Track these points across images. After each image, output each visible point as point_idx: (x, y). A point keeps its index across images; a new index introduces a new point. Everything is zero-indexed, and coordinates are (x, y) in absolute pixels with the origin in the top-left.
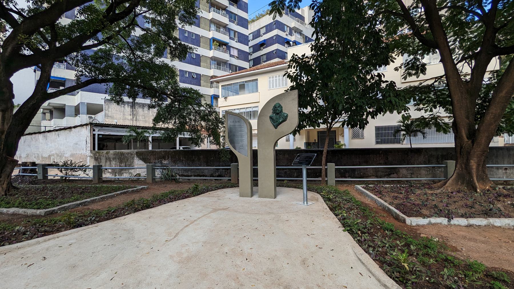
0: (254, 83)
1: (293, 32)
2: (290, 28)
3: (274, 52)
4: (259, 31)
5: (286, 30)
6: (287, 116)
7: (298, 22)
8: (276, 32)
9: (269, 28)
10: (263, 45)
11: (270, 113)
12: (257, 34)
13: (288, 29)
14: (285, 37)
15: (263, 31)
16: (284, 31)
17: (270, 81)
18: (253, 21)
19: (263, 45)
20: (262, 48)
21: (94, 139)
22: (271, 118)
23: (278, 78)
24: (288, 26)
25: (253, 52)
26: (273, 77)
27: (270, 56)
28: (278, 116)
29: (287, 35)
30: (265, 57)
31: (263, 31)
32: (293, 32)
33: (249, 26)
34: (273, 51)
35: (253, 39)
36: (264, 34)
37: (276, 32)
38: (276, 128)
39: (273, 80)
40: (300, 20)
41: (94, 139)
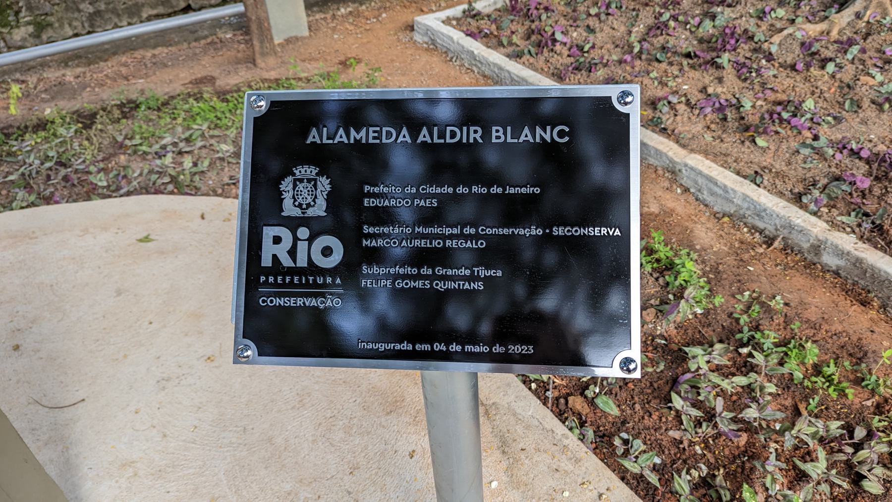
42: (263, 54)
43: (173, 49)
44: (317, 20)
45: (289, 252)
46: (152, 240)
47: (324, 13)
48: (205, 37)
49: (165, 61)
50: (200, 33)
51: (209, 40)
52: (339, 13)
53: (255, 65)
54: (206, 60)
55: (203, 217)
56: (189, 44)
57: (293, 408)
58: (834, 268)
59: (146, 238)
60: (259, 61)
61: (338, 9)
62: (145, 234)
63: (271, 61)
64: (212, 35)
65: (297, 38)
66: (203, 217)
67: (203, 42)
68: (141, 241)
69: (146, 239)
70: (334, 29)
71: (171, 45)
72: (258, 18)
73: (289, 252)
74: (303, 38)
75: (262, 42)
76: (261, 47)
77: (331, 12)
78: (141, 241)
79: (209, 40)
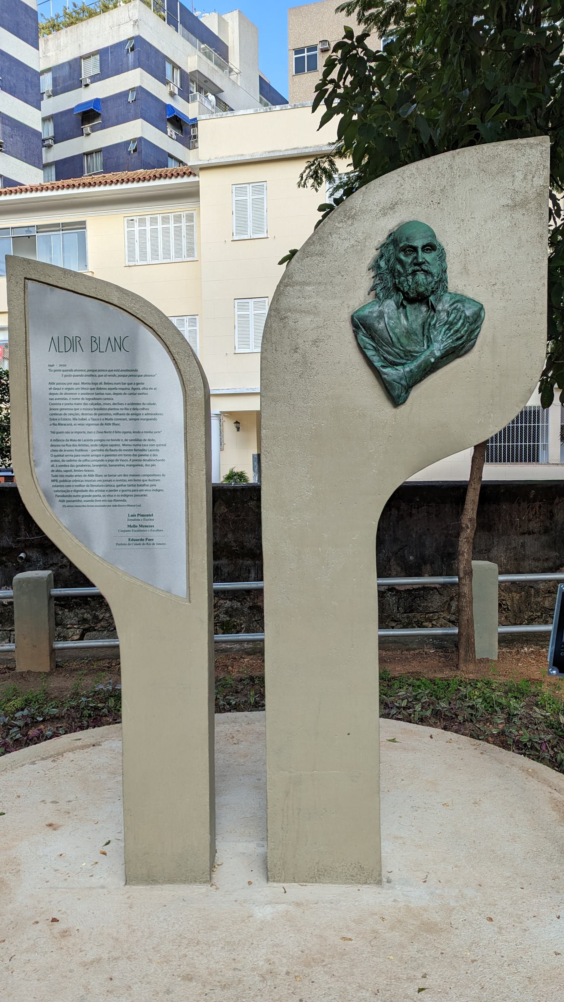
0: (73, 236)
1: (193, 88)
2: (183, 74)
3: (132, 147)
4: (75, 65)
5: (169, 77)
6: (477, 319)
7: (210, 58)
8: (134, 78)
9: (112, 60)
10: (89, 115)
11: (356, 289)
12: (69, 76)
13: (177, 74)
14: (168, 100)
15: (90, 68)
16: (166, 82)
17: (131, 235)
18: (54, 27)
19: (89, 115)
20: (87, 128)
21: (537, 458)
22: (361, 325)
23: (160, 226)
24: (175, 66)
25: (57, 139)
26: (142, 222)
27: (115, 160)
28: (417, 315)
29: (172, 94)
30: (98, 160)
31: (90, 68)
32: (193, 88)
33: (41, 42)
34: (127, 143)
35: (55, 93)
36: (95, 79)
37: (134, 78)
38: (396, 400)
39: (142, 233)
40: (214, 55)
41: (537, 458)
42: (466, 661)
43: (390, 653)
44: (503, 652)
45: (419, 989)
46: (396, 742)
47: (510, 648)
48: (414, 649)
49: (386, 659)
50: (410, 646)
51: (417, 652)
52: (522, 651)
53: (457, 668)
54: (414, 663)
55: (431, 737)
56: (402, 652)
57: (508, 841)
58: (86, 187)
59: (394, 739)
60: (462, 665)
61: (522, 648)
62: (393, 738)
63: (471, 667)
64: (419, 649)
65: (488, 660)
66: (431, 737)
67: (412, 652)
68: (390, 740)
69: (393, 741)
70: (518, 660)
71: (388, 650)
72: (468, 635)
73: (419, 989)
74: (492, 661)
75: (466, 652)
76: (466, 655)
77: (516, 649)
78: (390, 740)
79: (417, 652)
